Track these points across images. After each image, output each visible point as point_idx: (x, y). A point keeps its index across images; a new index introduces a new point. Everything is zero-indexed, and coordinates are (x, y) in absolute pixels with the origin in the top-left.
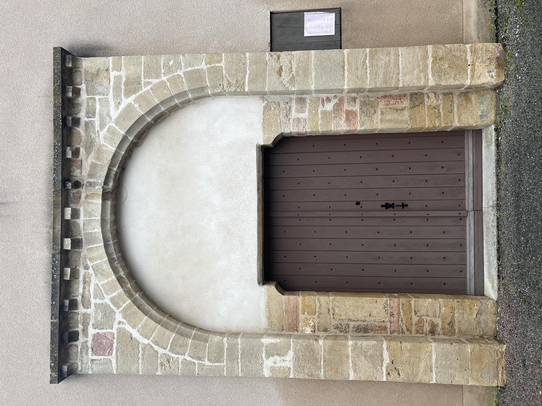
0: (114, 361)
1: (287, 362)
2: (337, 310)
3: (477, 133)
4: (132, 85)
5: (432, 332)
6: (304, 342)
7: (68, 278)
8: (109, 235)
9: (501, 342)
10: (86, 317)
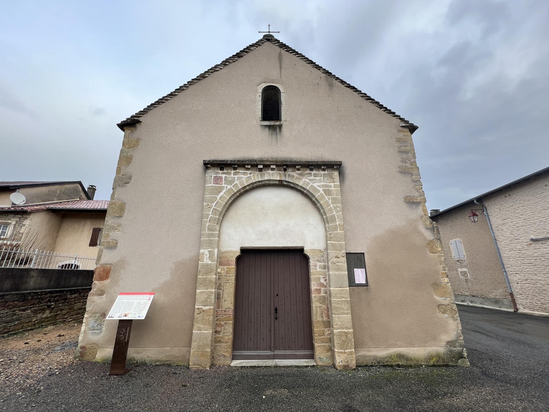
0: (211, 185)
1: (206, 260)
2: (228, 284)
3: (312, 357)
4: (328, 192)
5: (216, 332)
6: (214, 269)
7: (246, 166)
8: (264, 183)
9: (210, 367)
10: (230, 174)
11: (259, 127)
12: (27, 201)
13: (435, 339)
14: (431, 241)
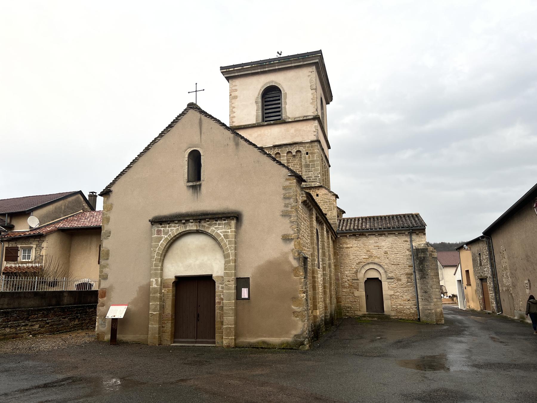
3: (214, 343)
4: (226, 236)
9: (159, 345)
11: (186, 188)
12: (40, 224)
13: (287, 333)
14: (296, 268)
